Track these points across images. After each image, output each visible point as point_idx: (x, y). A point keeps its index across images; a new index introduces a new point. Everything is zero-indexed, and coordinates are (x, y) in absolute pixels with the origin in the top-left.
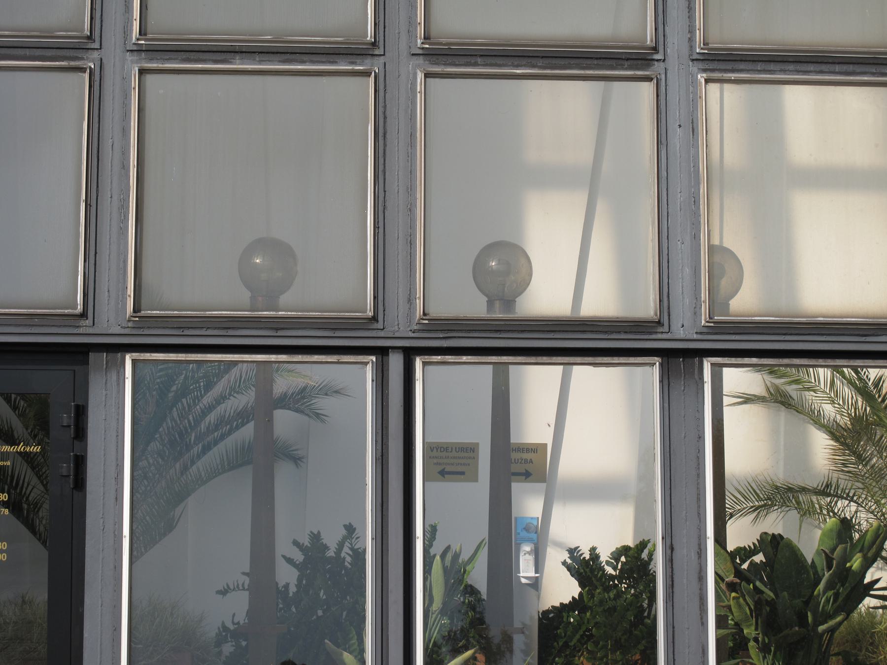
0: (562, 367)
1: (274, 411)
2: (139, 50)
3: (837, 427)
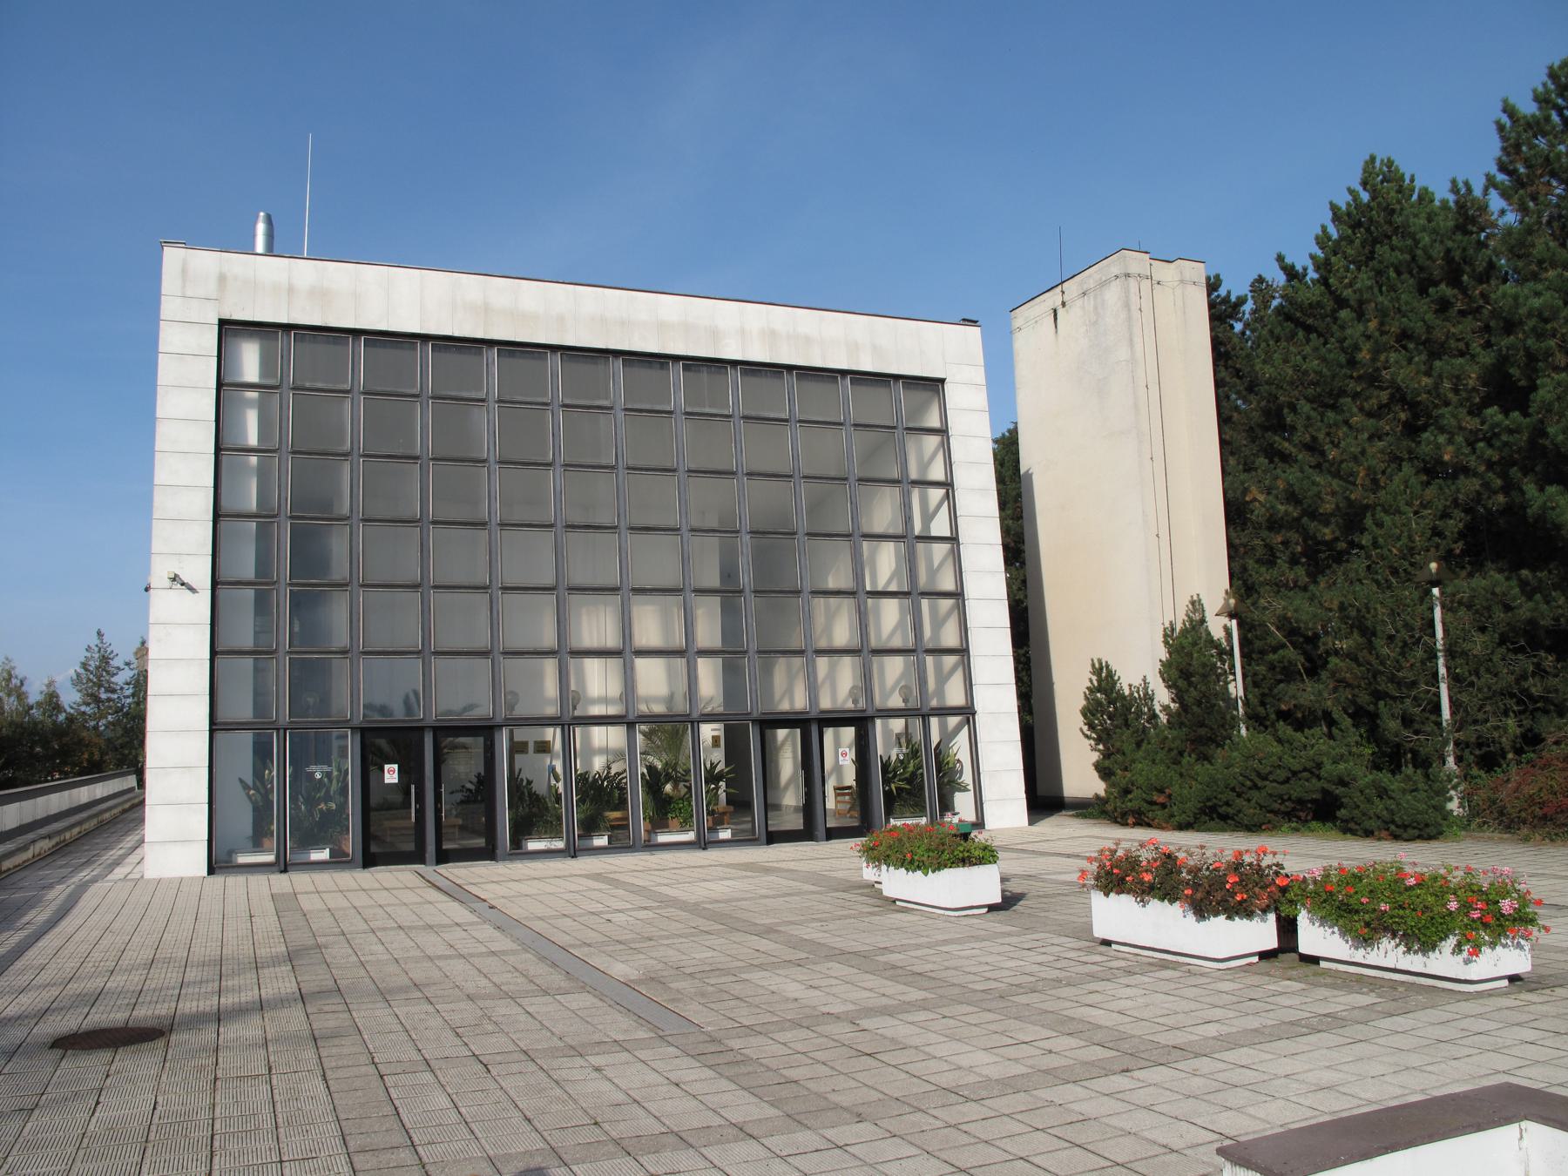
0: (934, 533)
1: (1000, 901)
2: (502, 653)
3: (1107, 677)
